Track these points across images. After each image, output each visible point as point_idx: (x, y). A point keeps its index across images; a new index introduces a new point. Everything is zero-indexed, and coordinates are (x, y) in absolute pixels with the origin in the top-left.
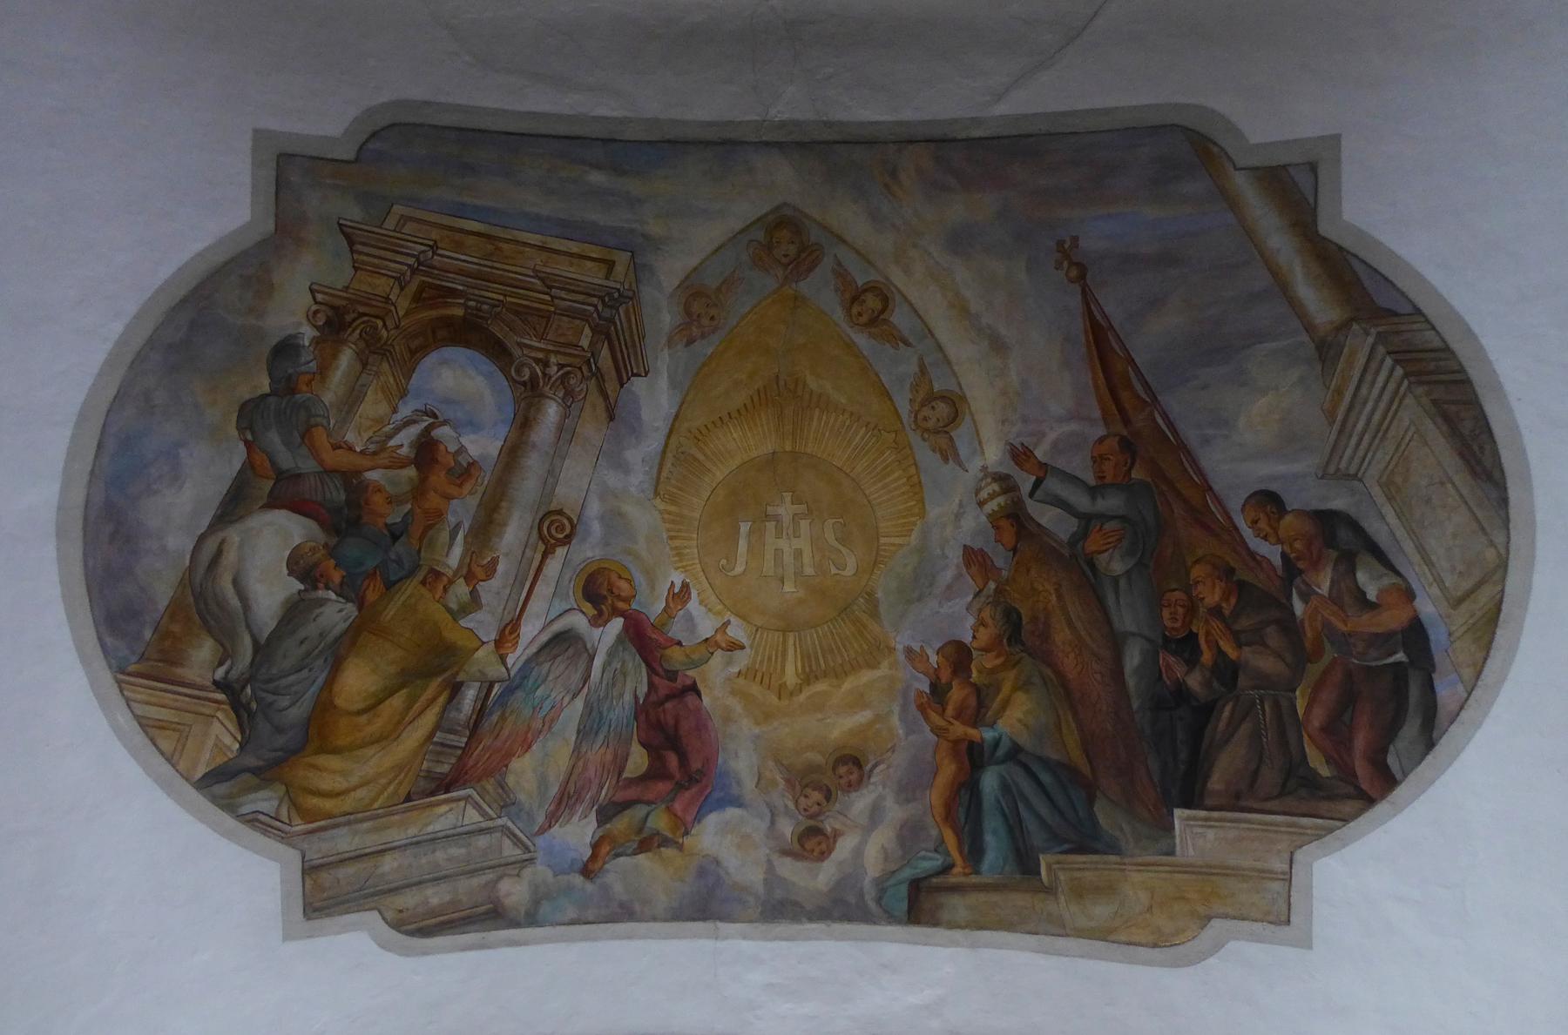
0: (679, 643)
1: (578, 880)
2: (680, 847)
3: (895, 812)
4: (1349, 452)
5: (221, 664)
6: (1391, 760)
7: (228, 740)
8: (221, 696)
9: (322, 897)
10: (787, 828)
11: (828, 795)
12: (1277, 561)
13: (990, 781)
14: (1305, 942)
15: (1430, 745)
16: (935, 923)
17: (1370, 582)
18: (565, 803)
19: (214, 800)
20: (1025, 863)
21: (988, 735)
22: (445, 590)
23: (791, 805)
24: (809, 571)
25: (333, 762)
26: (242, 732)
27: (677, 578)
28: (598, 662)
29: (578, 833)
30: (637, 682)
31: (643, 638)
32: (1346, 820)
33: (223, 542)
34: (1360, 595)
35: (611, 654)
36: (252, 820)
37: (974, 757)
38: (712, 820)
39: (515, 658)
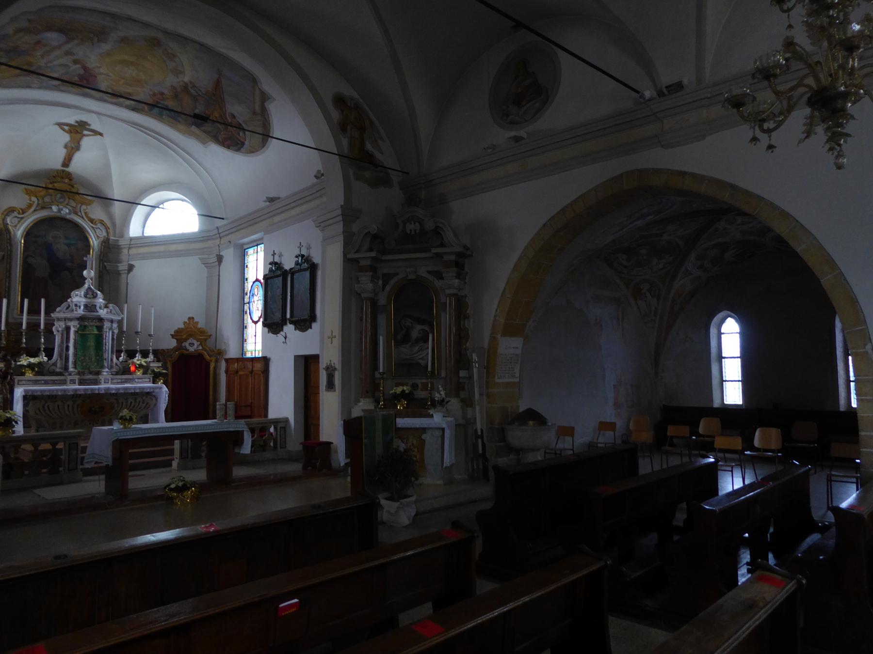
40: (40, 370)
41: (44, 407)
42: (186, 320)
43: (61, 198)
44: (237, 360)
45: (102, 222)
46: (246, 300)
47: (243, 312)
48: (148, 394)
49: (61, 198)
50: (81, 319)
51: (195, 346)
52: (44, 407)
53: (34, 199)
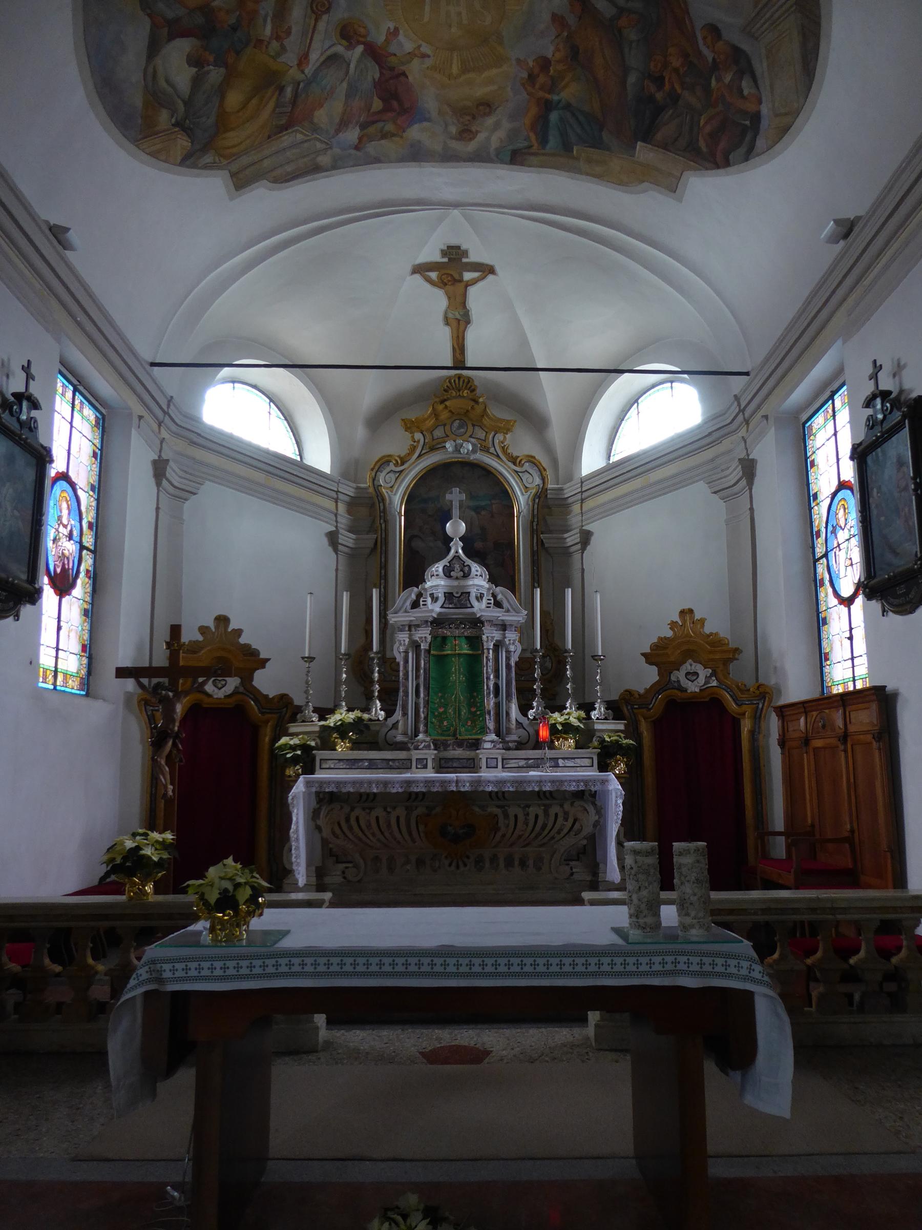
0: (395, 55)
1: (353, 152)
2: (402, 137)
3: (506, 125)
4: (758, 25)
5: (172, 117)
6: (731, 157)
7: (185, 143)
8: (177, 129)
9: (241, 182)
10: (453, 130)
11: (474, 118)
12: (710, 60)
13: (554, 117)
14: (680, 200)
15: (747, 159)
16: (522, 165)
17: (746, 86)
18: (343, 124)
19: (188, 167)
20: (567, 147)
21: (555, 98)
22: (267, 48)
23: (455, 121)
24: (465, 22)
25: (231, 134)
26: (189, 137)
27: (392, 25)
28: (352, 66)
29: (352, 135)
30: (373, 72)
31: (374, 53)
32: (707, 169)
33: (154, 67)
34: (741, 91)
35: (359, 61)
36: (206, 167)
37: (547, 106)
38: (416, 126)
39: (309, 70)
40: (364, 736)
41: (348, 820)
42: (676, 618)
43: (460, 427)
44: (804, 707)
45: (532, 460)
46: (820, 550)
47: (816, 583)
48: (579, 795)
49: (460, 427)
50: (437, 622)
51: (701, 680)
52: (348, 820)
53: (418, 436)
